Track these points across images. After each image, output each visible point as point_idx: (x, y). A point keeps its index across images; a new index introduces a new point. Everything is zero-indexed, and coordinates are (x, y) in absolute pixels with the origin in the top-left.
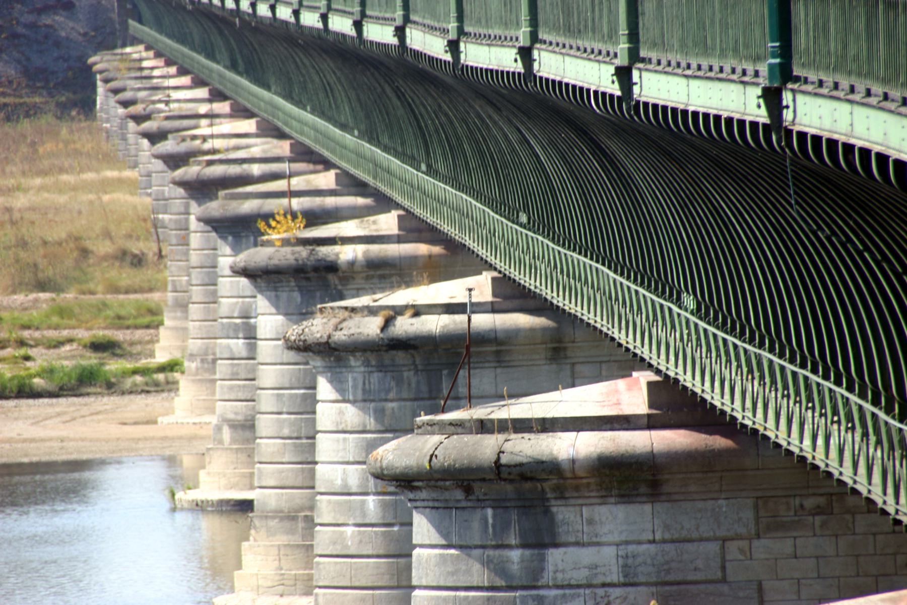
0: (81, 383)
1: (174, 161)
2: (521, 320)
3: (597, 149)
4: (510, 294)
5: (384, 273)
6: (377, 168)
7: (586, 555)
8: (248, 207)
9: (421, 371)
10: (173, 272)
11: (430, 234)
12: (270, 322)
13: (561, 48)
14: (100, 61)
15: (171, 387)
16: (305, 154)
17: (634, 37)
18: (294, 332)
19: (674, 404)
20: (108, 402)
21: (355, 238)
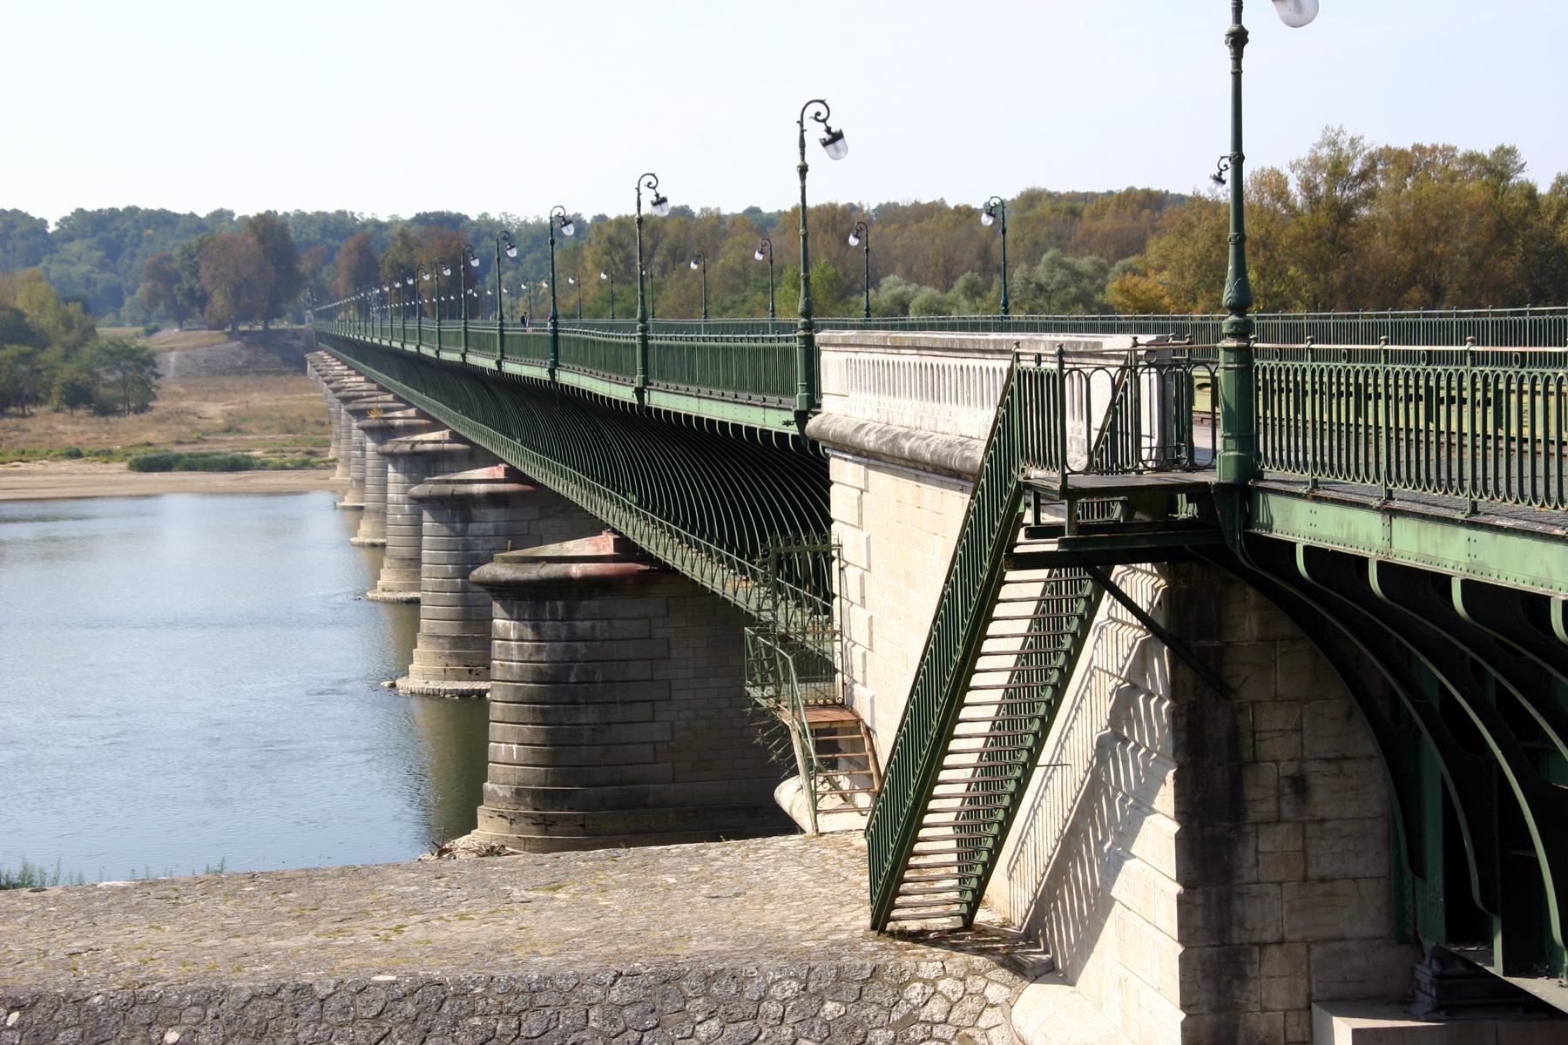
0: (303, 466)
1: (336, 390)
2: (459, 446)
3: (488, 389)
4: (456, 437)
5: (411, 429)
6: (408, 393)
7: (483, 526)
8: (362, 406)
9: (422, 464)
10: (335, 429)
11: (427, 416)
12: (370, 445)
13: (476, 355)
14: (308, 356)
15: (334, 467)
16: (382, 389)
17: (502, 351)
18: (380, 449)
19: (513, 475)
20: (312, 472)
21: (399, 417)
